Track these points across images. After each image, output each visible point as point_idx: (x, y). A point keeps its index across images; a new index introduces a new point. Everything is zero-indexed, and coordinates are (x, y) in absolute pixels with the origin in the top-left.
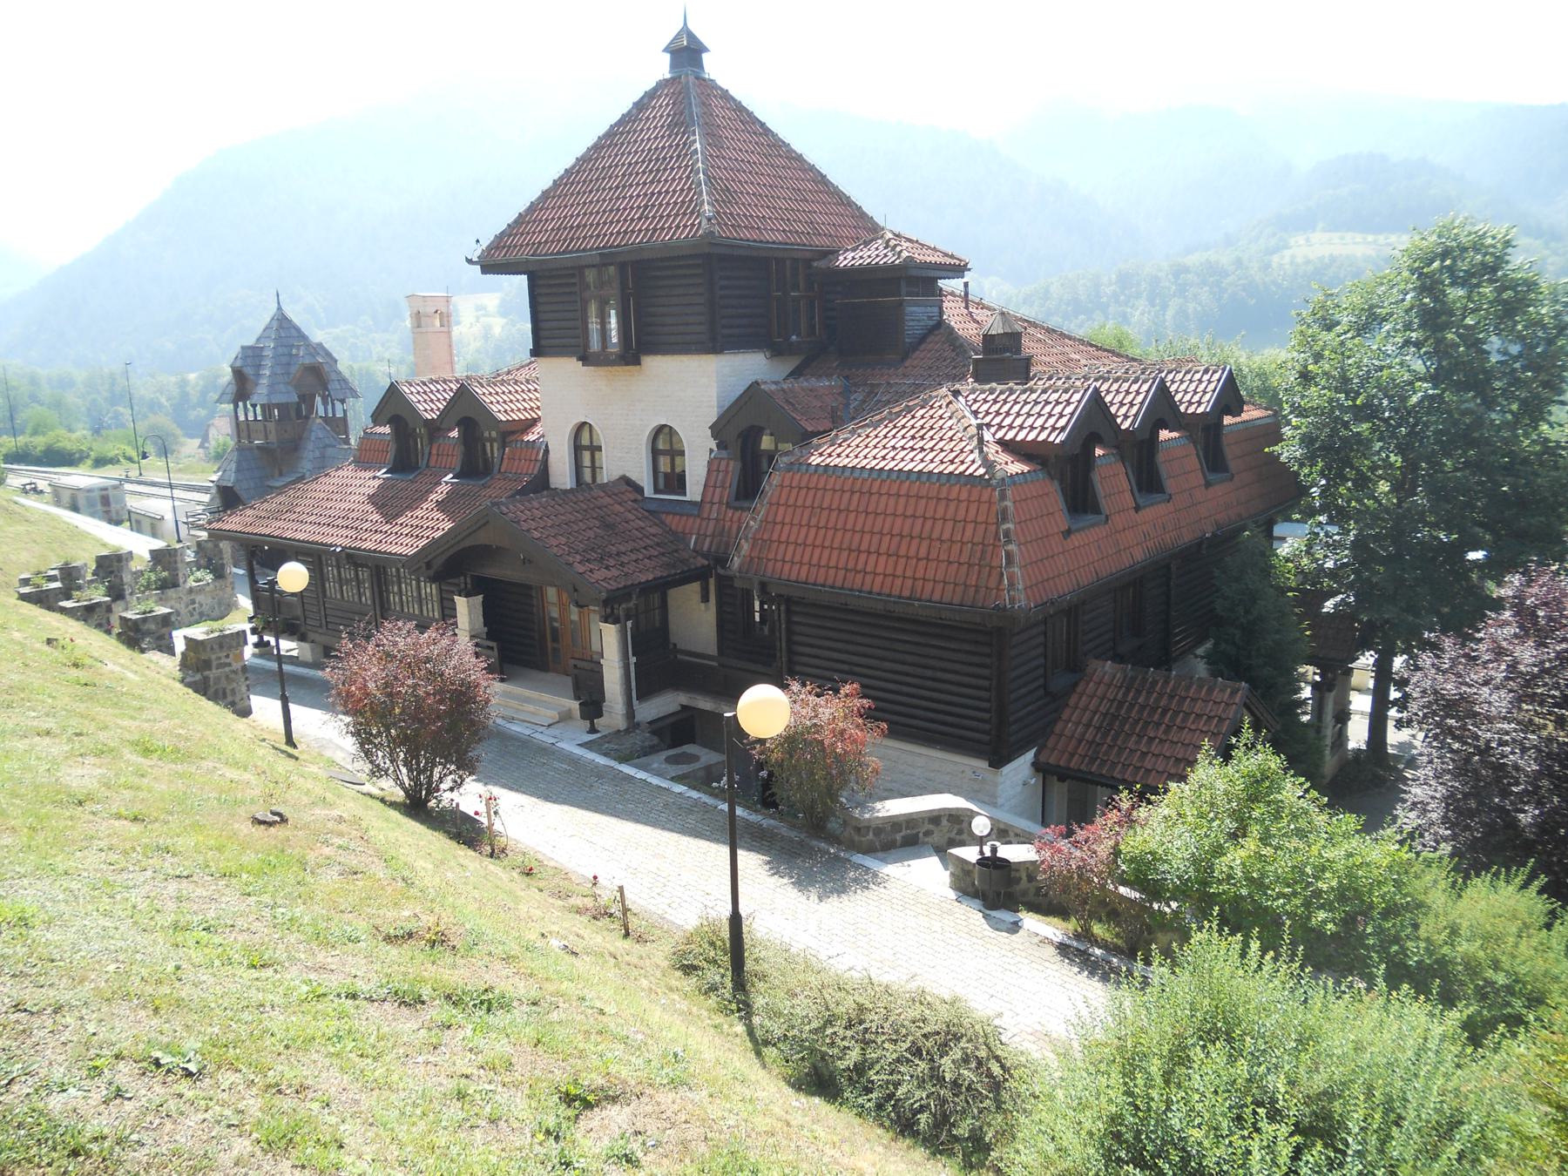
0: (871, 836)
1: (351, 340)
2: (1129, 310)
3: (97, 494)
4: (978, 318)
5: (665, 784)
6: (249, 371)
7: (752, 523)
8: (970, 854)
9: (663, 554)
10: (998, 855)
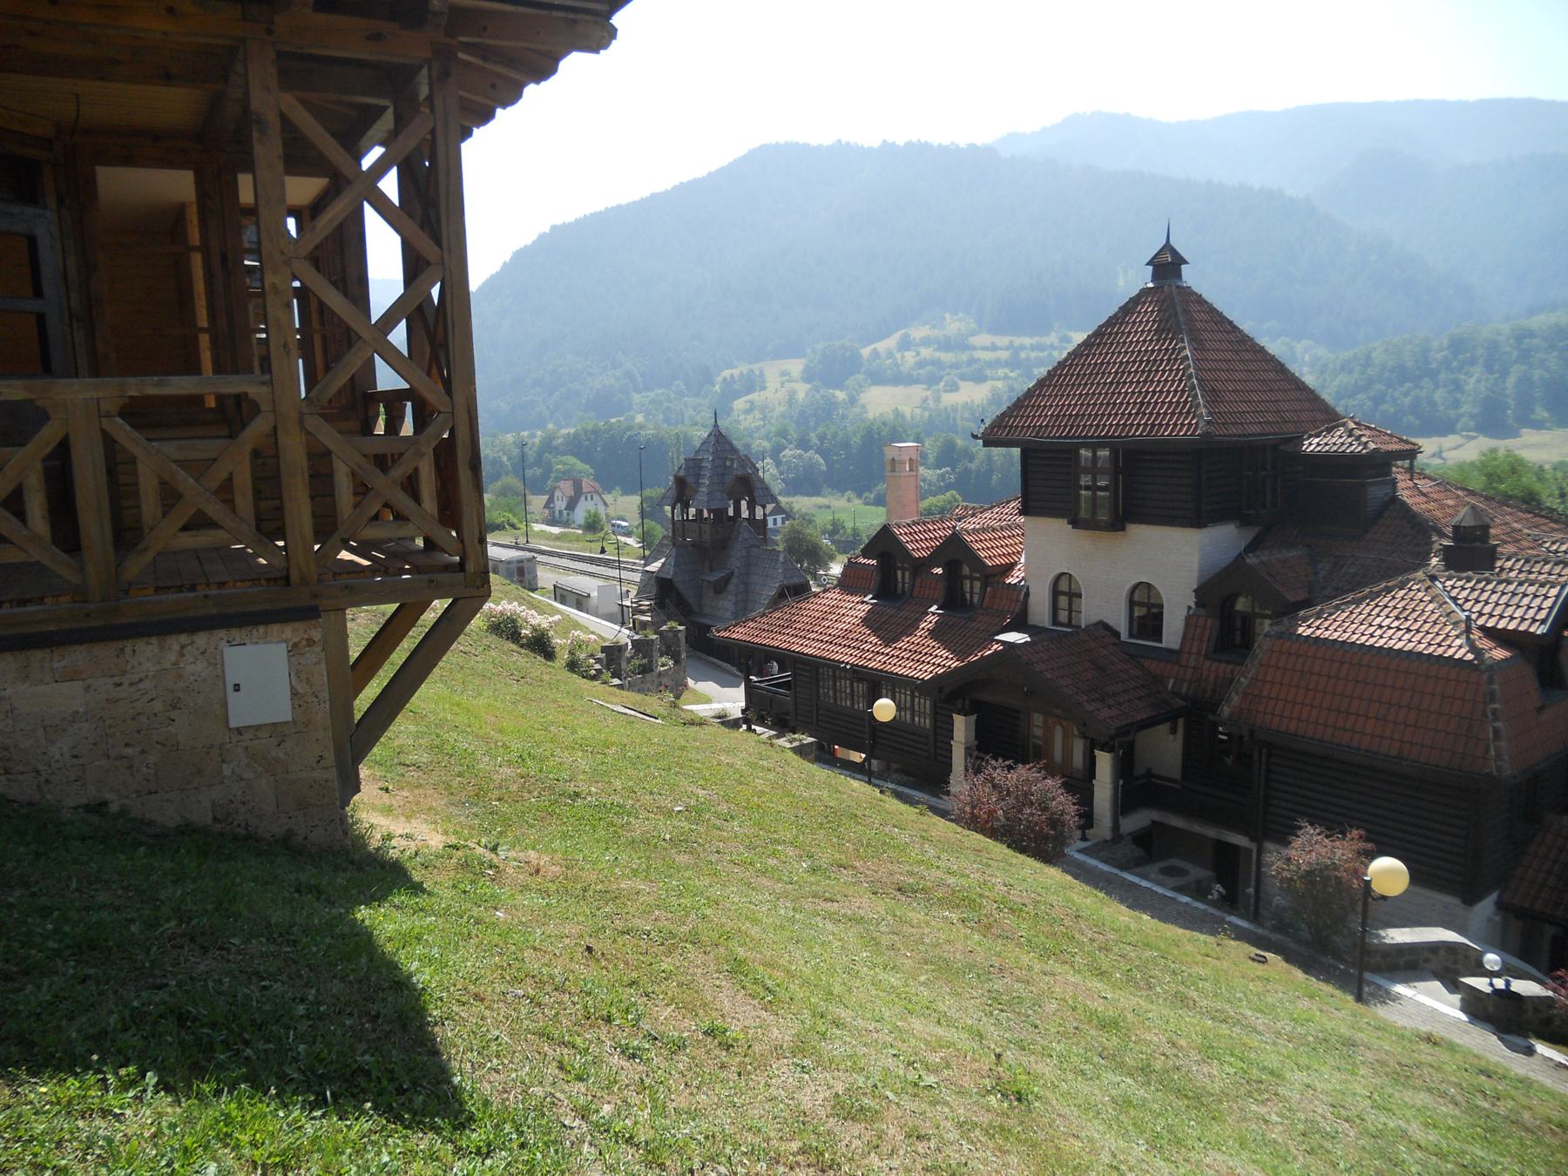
0: (1378, 959)
1: (666, 404)
2: (1462, 377)
3: (514, 566)
4: (1424, 491)
5: (1170, 894)
6: (690, 480)
7: (1242, 679)
8: (1481, 983)
9: (1149, 695)
10: (1512, 989)
